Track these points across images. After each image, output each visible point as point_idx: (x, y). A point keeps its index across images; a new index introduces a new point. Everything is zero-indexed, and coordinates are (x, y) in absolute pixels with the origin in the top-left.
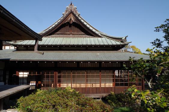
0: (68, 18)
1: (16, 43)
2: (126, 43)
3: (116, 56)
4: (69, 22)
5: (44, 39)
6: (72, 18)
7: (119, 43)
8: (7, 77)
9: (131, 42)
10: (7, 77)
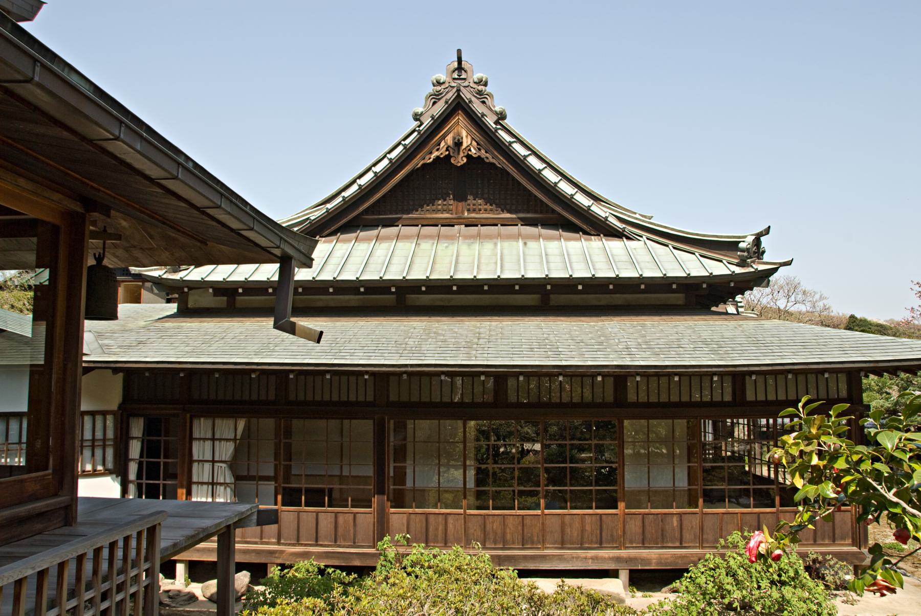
0: (444, 137)
1: (176, 271)
2: (761, 267)
3: (704, 342)
4: (448, 157)
5: (322, 249)
6: (464, 133)
7: (719, 268)
8: (135, 450)
9: (788, 263)
10: (135, 450)
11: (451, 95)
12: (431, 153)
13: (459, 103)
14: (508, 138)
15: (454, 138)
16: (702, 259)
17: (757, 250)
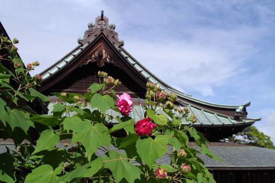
0: (94, 53)
2: (247, 121)
6: (104, 51)
7: (228, 121)
11: (98, 33)
12: (87, 60)
13: (102, 37)
14: (125, 55)
15: (99, 54)
16: (218, 117)
17: (244, 112)
